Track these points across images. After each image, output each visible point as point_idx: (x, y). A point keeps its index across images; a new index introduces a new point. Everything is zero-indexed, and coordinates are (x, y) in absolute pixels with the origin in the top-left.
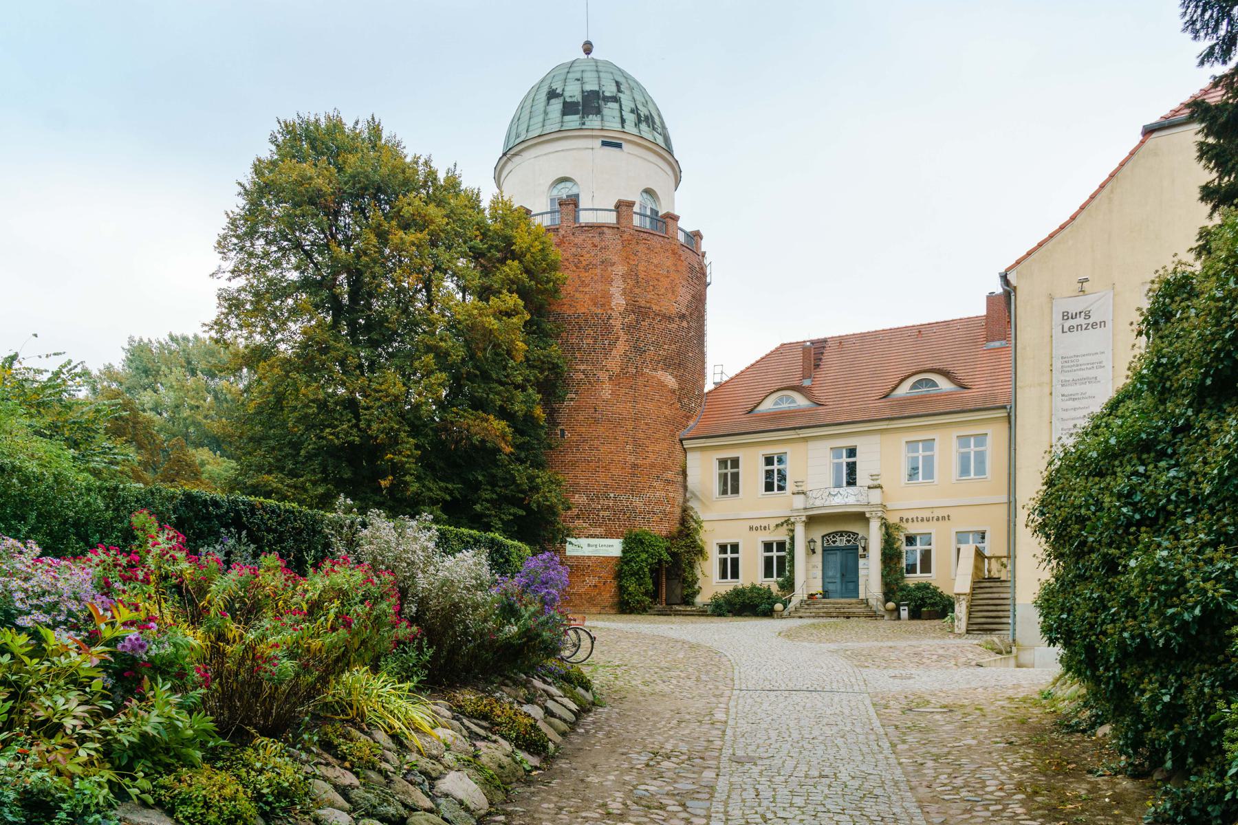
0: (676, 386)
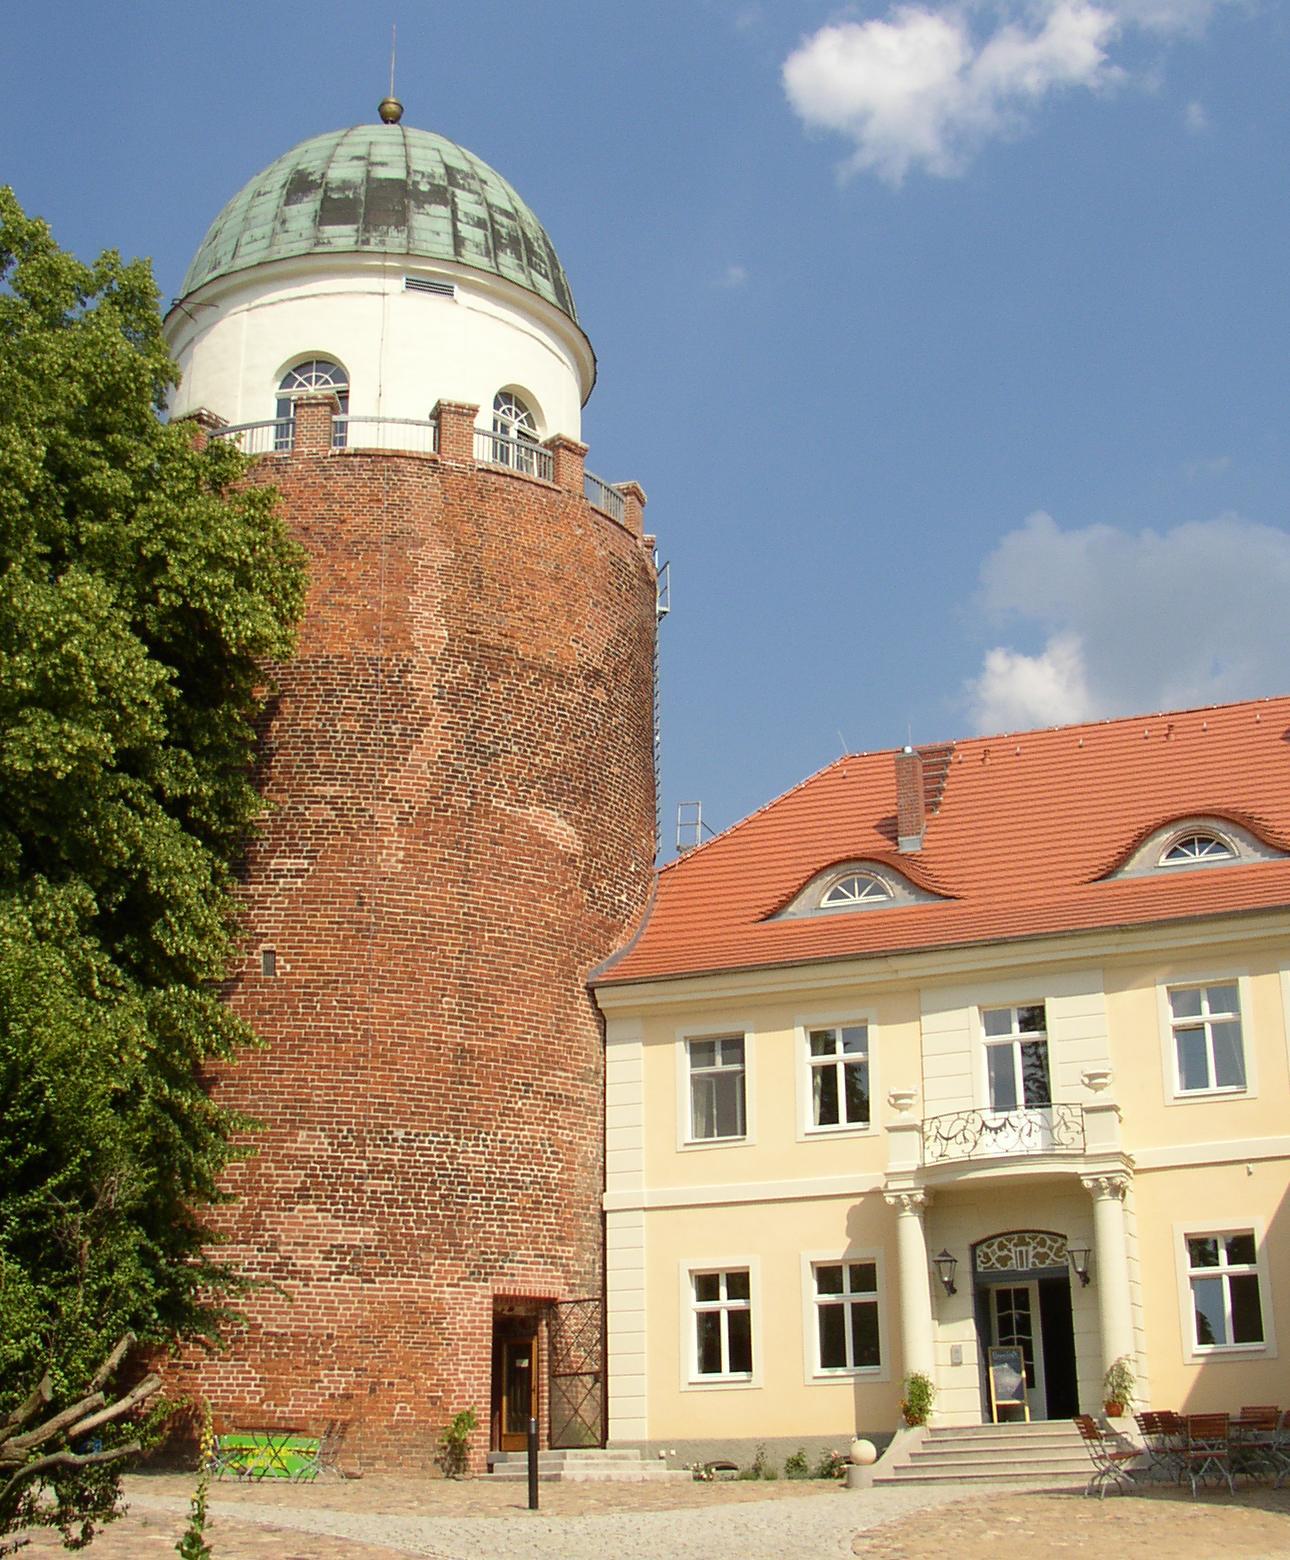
0: (576, 846)
